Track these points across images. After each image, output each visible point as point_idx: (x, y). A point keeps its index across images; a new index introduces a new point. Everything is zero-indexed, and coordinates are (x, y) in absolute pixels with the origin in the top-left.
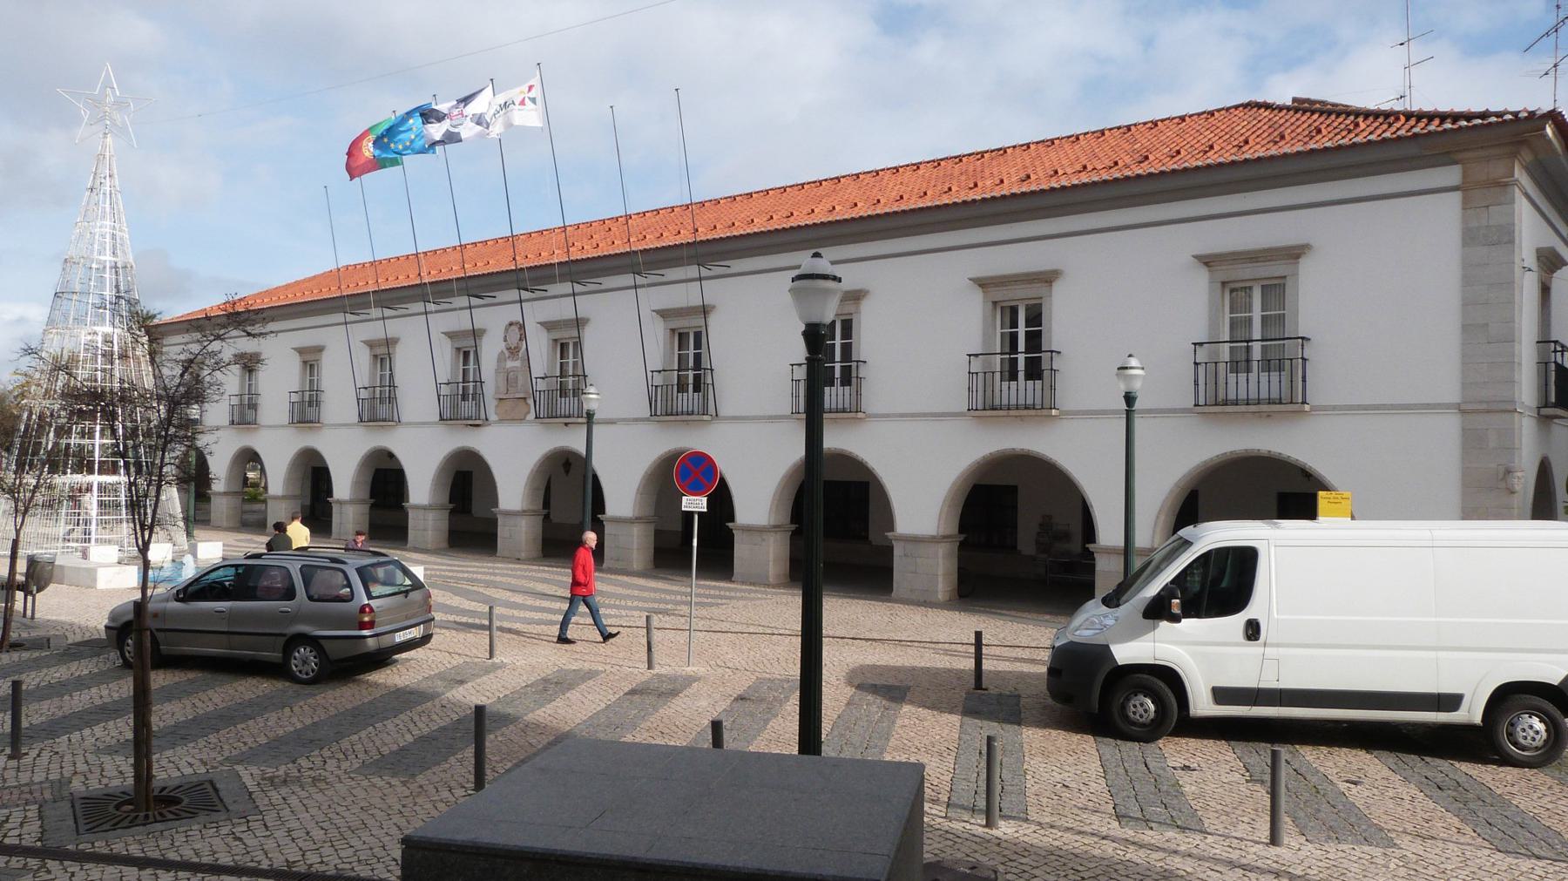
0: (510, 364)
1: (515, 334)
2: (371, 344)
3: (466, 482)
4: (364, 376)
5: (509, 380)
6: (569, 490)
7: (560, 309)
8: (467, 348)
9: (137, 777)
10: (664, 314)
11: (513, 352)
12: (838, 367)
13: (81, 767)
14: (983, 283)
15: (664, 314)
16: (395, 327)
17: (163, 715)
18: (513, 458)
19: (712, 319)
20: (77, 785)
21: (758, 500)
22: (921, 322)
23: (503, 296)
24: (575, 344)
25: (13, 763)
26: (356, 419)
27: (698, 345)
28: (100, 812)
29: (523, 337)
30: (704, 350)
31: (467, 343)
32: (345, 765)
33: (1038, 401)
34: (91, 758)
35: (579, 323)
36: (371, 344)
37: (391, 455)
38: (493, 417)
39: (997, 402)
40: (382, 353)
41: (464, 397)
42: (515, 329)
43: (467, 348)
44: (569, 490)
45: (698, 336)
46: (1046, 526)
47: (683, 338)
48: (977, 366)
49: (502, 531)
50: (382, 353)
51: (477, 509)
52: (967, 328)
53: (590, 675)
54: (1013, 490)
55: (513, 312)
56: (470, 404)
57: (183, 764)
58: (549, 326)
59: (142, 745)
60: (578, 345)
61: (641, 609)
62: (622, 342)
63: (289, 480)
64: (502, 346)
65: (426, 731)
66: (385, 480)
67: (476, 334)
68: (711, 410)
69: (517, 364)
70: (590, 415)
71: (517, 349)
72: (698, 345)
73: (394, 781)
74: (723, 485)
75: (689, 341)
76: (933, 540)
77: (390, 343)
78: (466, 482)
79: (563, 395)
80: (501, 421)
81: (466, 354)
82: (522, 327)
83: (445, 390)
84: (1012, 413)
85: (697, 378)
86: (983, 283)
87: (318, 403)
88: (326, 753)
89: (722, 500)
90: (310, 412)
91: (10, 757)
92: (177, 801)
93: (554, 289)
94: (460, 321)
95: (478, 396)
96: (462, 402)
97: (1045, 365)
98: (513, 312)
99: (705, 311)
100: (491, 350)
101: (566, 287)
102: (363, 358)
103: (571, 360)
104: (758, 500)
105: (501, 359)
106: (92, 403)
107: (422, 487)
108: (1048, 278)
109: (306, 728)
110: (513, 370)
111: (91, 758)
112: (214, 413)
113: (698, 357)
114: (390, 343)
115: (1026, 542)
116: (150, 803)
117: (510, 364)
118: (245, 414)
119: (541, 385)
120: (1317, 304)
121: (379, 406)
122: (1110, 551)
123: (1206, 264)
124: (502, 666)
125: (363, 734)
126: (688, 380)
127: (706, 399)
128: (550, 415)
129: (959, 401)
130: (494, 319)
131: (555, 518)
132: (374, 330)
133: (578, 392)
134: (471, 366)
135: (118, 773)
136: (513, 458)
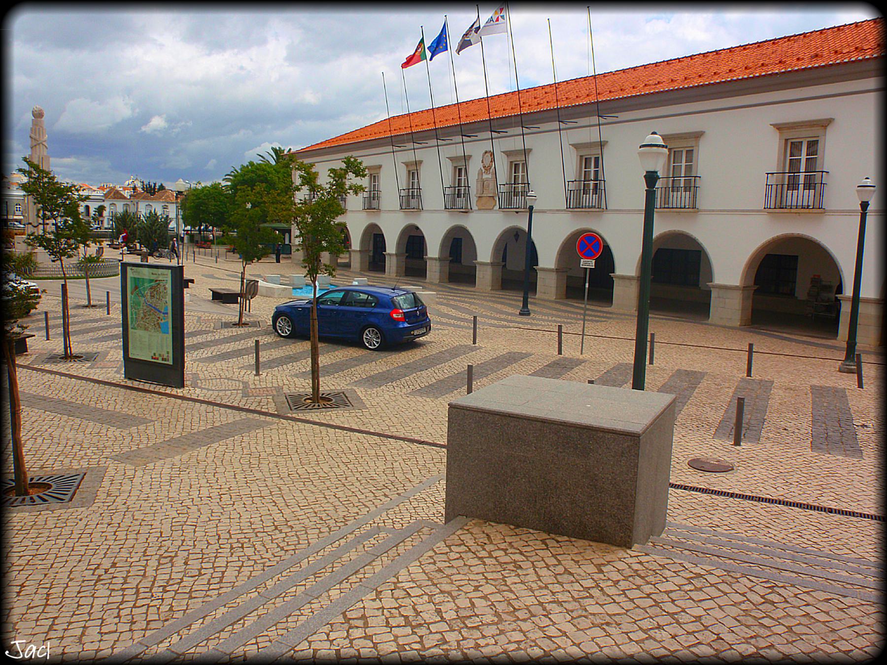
0: (485, 176)
1: (488, 158)
2: (407, 164)
3: (458, 244)
4: (403, 184)
5: (483, 184)
6: (517, 248)
7: (516, 144)
8: (460, 169)
9: (313, 388)
10: (576, 146)
11: (487, 169)
12: (802, 176)
13: (286, 382)
14: (779, 127)
15: (576, 146)
16: (420, 155)
17: (323, 360)
18: (486, 230)
19: (605, 151)
20: (285, 390)
21: (627, 260)
22: (551, 163)
23: (482, 135)
24: (597, 160)
25: (257, 378)
26: (399, 207)
27: (596, 166)
28: (296, 402)
29: (493, 160)
30: (600, 168)
31: (520, 159)
32: (404, 390)
33: (811, 203)
34: (289, 378)
35: (526, 152)
36: (407, 164)
37: (417, 228)
38: (475, 208)
39: (800, 203)
40: (413, 170)
41: (459, 196)
42: (489, 155)
43: (460, 169)
44: (517, 248)
45: (597, 160)
46: (815, 281)
47: (796, 147)
48: (772, 180)
49: (478, 274)
50: (413, 170)
51: (465, 261)
52: (768, 154)
53: (528, 355)
54: (795, 258)
55: (487, 146)
56: (462, 199)
57: (329, 384)
58: (508, 154)
59: (315, 373)
60: (525, 165)
61: (555, 321)
62: (551, 163)
63: (399, 244)
64: (481, 165)
65: (442, 378)
66: (413, 241)
67: (466, 158)
68: (603, 206)
69: (490, 176)
70: (531, 208)
71: (490, 167)
72: (689, 159)
73: (428, 399)
74: (607, 250)
75: (591, 161)
76: (735, 288)
77: (418, 163)
78: (458, 244)
79: (516, 194)
80: (479, 209)
81: (460, 170)
82: (492, 154)
83: (448, 191)
84: (792, 211)
85: (596, 185)
86: (779, 127)
87: (378, 198)
88: (395, 384)
89: (606, 259)
90: (375, 203)
91: (255, 375)
92: (330, 400)
93: (511, 131)
94: (457, 151)
95: (467, 195)
96: (457, 197)
97: (818, 181)
98: (487, 146)
99: (602, 145)
100: (474, 168)
101: (519, 130)
102: (403, 172)
103: (520, 174)
104: (627, 260)
105: (481, 173)
106: (71, 210)
107: (433, 249)
108: (825, 124)
109: (384, 372)
110: (487, 180)
111: (289, 378)
112: (354, 202)
113: (596, 172)
114: (418, 163)
115: (802, 290)
116: (318, 399)
117: (485, 176)
118: (372, 204)
119: (503, 189)
120: (707, 161)
121: (411, 199)
122: (847, 299)
123: (778, 129)
124: (480, 348)
125: (411, 377)
126: (589, 187)
127: (600, 198)
128: (508, 206)
129: (759, 203)
130: (476, 149)
131: (509, 267)
132: (410, 156)
133: (524, 193)
134: (416, 181)
135: (304, 386)
136: (486, 230)
